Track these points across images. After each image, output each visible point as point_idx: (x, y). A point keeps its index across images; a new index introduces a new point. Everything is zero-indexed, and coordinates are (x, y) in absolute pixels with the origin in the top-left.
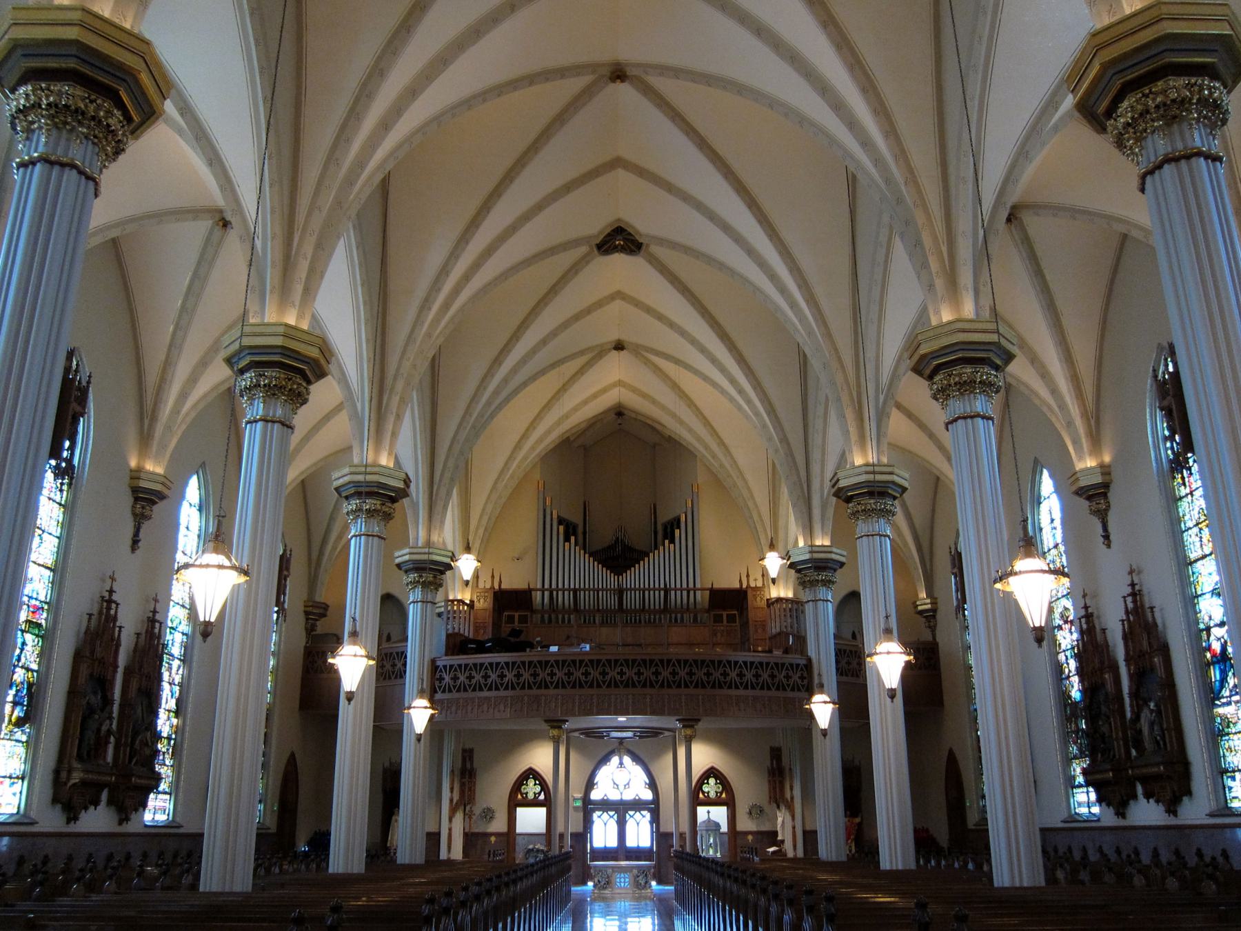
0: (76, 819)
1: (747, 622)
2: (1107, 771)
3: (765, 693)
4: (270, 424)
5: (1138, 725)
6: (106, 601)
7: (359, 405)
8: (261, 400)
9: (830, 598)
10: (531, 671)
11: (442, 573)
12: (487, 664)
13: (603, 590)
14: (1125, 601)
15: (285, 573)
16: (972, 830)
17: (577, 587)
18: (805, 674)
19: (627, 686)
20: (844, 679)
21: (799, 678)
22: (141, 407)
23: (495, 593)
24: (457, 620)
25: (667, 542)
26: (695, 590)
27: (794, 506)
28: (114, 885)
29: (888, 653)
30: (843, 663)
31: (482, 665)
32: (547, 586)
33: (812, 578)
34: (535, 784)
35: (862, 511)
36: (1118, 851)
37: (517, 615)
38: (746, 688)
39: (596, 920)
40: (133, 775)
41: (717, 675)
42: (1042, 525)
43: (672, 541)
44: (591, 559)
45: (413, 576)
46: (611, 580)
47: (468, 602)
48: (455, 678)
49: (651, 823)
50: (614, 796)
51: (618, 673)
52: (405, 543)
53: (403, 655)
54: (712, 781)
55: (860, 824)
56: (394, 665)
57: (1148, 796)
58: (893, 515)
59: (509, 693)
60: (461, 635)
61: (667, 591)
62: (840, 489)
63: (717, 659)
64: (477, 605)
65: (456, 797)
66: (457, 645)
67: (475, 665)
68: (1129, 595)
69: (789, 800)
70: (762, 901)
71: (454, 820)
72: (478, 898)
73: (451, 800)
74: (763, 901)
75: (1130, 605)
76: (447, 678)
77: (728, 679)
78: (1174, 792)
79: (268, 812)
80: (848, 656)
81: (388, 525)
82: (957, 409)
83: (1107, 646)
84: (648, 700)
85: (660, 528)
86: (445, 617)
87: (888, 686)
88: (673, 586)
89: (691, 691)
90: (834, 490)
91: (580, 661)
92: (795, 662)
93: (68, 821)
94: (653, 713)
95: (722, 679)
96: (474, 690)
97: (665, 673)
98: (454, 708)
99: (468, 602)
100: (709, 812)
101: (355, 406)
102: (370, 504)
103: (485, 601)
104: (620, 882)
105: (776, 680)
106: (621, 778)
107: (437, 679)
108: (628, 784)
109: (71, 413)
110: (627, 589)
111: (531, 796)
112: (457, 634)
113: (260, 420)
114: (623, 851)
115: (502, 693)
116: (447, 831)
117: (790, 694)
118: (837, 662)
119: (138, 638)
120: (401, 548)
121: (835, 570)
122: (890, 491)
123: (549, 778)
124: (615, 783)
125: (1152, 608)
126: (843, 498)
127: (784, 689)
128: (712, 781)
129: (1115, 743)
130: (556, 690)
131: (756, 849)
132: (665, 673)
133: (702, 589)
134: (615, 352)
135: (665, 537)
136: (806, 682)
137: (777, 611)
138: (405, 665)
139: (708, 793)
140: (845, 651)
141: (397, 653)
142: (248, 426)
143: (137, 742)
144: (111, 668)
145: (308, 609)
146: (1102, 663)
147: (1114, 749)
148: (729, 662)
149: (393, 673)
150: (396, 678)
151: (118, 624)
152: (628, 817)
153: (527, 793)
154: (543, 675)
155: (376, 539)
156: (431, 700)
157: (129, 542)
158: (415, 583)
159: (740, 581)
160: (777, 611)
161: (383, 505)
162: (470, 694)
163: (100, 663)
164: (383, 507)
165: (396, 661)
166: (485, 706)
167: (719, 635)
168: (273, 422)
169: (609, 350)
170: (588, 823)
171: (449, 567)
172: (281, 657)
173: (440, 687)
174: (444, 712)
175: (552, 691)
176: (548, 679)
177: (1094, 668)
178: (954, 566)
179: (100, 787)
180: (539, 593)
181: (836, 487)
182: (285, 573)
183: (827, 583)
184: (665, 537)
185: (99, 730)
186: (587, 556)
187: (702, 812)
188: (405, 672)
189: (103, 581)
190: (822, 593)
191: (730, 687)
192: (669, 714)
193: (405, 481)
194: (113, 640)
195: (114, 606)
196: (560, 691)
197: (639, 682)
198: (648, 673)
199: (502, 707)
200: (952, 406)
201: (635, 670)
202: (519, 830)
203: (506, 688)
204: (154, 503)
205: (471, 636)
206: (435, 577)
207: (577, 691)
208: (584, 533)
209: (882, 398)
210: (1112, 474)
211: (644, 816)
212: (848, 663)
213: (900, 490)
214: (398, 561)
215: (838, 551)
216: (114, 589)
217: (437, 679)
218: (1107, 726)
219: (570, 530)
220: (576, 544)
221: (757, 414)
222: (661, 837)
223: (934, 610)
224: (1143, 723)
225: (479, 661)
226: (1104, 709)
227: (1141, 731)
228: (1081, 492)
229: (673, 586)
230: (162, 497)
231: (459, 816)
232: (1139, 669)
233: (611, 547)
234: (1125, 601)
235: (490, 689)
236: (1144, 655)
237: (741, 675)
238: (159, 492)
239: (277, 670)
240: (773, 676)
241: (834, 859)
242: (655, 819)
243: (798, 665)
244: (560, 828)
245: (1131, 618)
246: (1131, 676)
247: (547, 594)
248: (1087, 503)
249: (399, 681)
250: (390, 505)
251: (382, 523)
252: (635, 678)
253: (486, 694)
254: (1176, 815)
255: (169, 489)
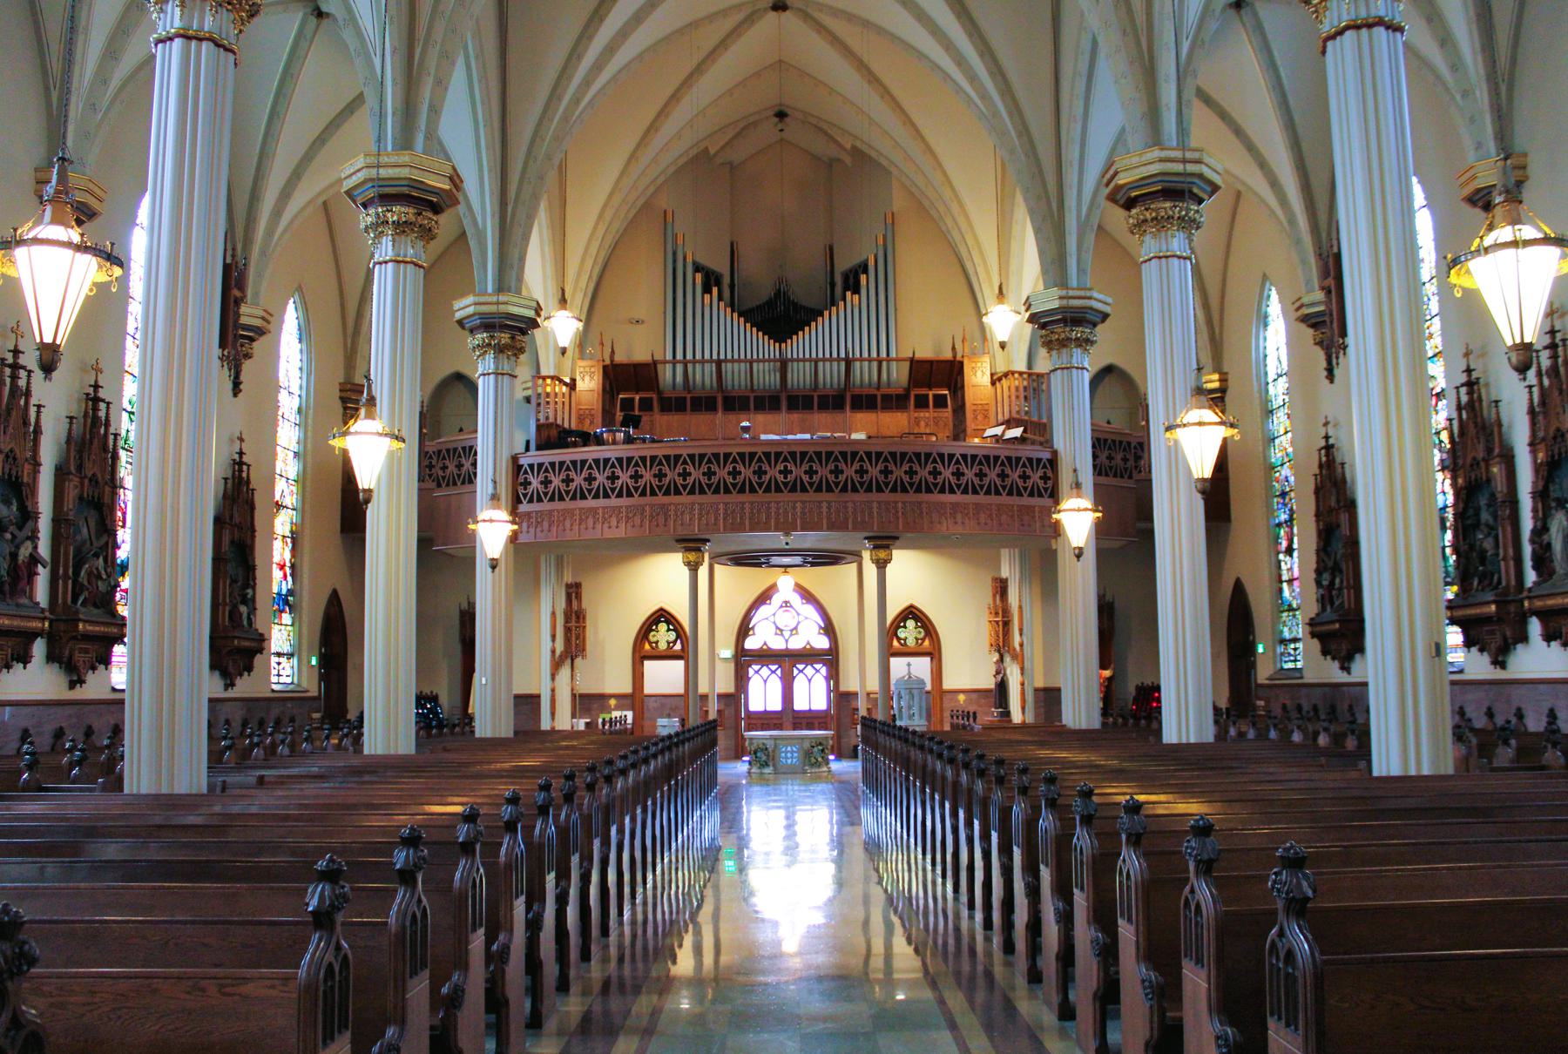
0: (232, 685)
1: (963, 405)
2: (1488, 603)
3: (993, 499)
4: (194, 43)
5: (1545, 537)
6: (91, 399)
7: (377, 61)
8: (390, 238)
9: (1086, 366)
10: (656, 470)
11: (524, 332)
12: (590, 461)
13: (758, 361)
14: (1458, 393)
15: (236, 293)
16: (1262, 686)
17: (722, 357)
18: (1050, 474)
19: (793, 490)
20: (1103, 480)
21: (1041, 478)
22: (45, 72)
23: (605, 367)
24: (552, 405)
25: (849, 294)
26: (889, 360)
27: (1037, 231)
28: (262, 752)
29: (1200, 424)
30: (1103, 457)
31: (584, 462)
32: (679, 356)
33: (1063, 336)
34: (669, 630)
35: (1153, 219)
36: (1490, 714)
37: (637, 397)
38: (965, 492)
39: (754, 808)
40: (80, 620)
41: (923, 473)
42: (1268, 352)
43: (856, 290)
44: (742, 319)
45: (481, 337)
46: (768, 348)
47: (567, 380)
48: (546, 482)
49: (827, 679)
50: (777, 644)
51: (780, 472)
52: (468, 289)
53: (471, 451)
54: (911, 624)
55: (1110, 679)
56: (460, 466)
57: (1548, 637)
58: (1198, 228)
59: (624, 501)
60: (558, 426)
61: (849, 362)
62: (1118, 188)
63: (923, 450)
64: (580, 385)
65: (560, 647)
66: (552, 436)
67: (574, 463)
68: (1462, 385)
69: (1018, 648)
70: (979, 786)
71: (557, 678)
72: (634, 766)
73: (553, 652)
74: (964, 778)
75: (1464, 399)
76: (535, 483)
77: (940, 479)
78: (1505, 639)
79: (305, 669)
80: (1110, 448)
81: (428, 246)
82: (1344, 13)
83: (1500, 425)
84: (825, 510)
85: (838, 279)
86: (534, 401)
87: (1075, 544)
88: (858, 355)
89: (887, 496)
90: (1107, 191)
91: (725, 454)
92: (1035, 455)
93: (72, 686)
94: (832, 527)
95: (931, 479)
96: (574, 498)
97: (850, 472)
98: (546, 524)
99: (567, 380)
100: (909, 665)
101: (370, 64)
102: (398, 212)
103: (592, 378)
104: (787, 758)
105: (1008, 482)
106: (786, 620)
107: (521, 484)
108: (796, 628)
109: (232, 300)
110: (792, 360)
111: (663, 646)
112: (552, 424)
113: (178, 35)
114: (790, 717)
115: (614, 502)
116: (549, 693)
117: (1026, 500)
118: (1095, 457)
119: (71, 423)
120: (463, 295)
121: (1095, 325)
122: (1195, 190)
123: (685, 620)
124: (777, 628)
125: (1343, 464)
126: (1122, 202)
127: (1020, 494)
128: (911, 624)
129: (1502, 563)
130: (691, 497)
131: (975, 713)
132: (850, 472)
133: (898, 360)
134: (773, 15)
135: (846, 289)
136: (1050, 484)
137: (1006, 390)
138: (474, 464)
139: (905, 639)
140: (1106, 440)
141: (464, 448)
142: (377, 267)
143: (83, 573)
144: (27, 466)
145: (344, 394)
146: (1489, 450)
147: (1499, 572)
148: (941, 456)
149: (459, 476)
150: (463, 483)
151: (34, 401)
152: (796, 672)
153: (657, 642)
154: (671, 475)
155: (410, 267)
156: (513, 512)
157: (230, 386)
158: (484, 347)
159: (954, 348)
160: (1006, 390)
161: (420, 214)
162: (568, 504)
163: (90, 480)
164: (419, 218)
165: (463, 460)
166: (590, 521)
167: (922, 423)
168: (200, 40)
169: (765, 10)
170: (741, 679)
171: (536, 325)
172: (309, 458)
173: (525, 495)
174: (532, 530)
175: (684, 499)
176: (680, 481)
177: (1474, 459)
178: (1325, 274)
179: (32, 636)
180: (669, 367)
181: (1112, 185)
182: (236, 293)
183: (1084, 343)
184: (846, 289)
185: (14, 556)
186: (736, 315)
187: (898, 666)
188: (475, 474)
189: (84, 370)
190: (1078, 357)
191: (942, 491)
192: (855, 529)
193: (451, 178)
194: (26, 423)
195: (245, 468)
196: (697, 498)
197: (811, 484)
198: (824, 472)
199: (614, 521)
200: (1335, 9)
201: (805, 467)
202: (648, 690)
203: (620, 495)
204: (252, 340)
205: (574, 427)
206: (513, 338)
207: (721, 498)
208: (732, 286)
209: (1186, 45)
210: (1529, 168)
211: (817, 671)
212: (1110, 458)
213: (1209, 189)
214: (458, 315)
215: (1101, 296)
216: (21, 348)
217: (521, 484)
218: (1490, 540)
219: (711, 280)
220: (720, 298)
221: (984, 96)
222: (842, 699)
223: (1223, 390)
224: (1554, 536)
225: (578, 457)
226: (1485, 516)
227: (1549, 545)
228: (1304, 319)
229: (858, 355)
230: (261, 332)
231: (565, 672)
232: (1553, 456)
233: (771, 304)
234: (1458, 393)
235: (596, 496)
236: (1478, 464)
237: (958, 474)
238: (258, 328)
239: (304, 478)
240: (1003, 476)
241: (1084, 726)
242: (834, 674)
243: (1039, 460)
244: (703, 688)
245: (1464, 416)
246: (1537, 468)
247: (679, 368)
248: (1310, 331)
249: (467, 488)
250: (430, 215)
251: (420, 244)
252: (806, 478)
253: (591, 503)
254: (1349, 673)
255: (268, 322)
